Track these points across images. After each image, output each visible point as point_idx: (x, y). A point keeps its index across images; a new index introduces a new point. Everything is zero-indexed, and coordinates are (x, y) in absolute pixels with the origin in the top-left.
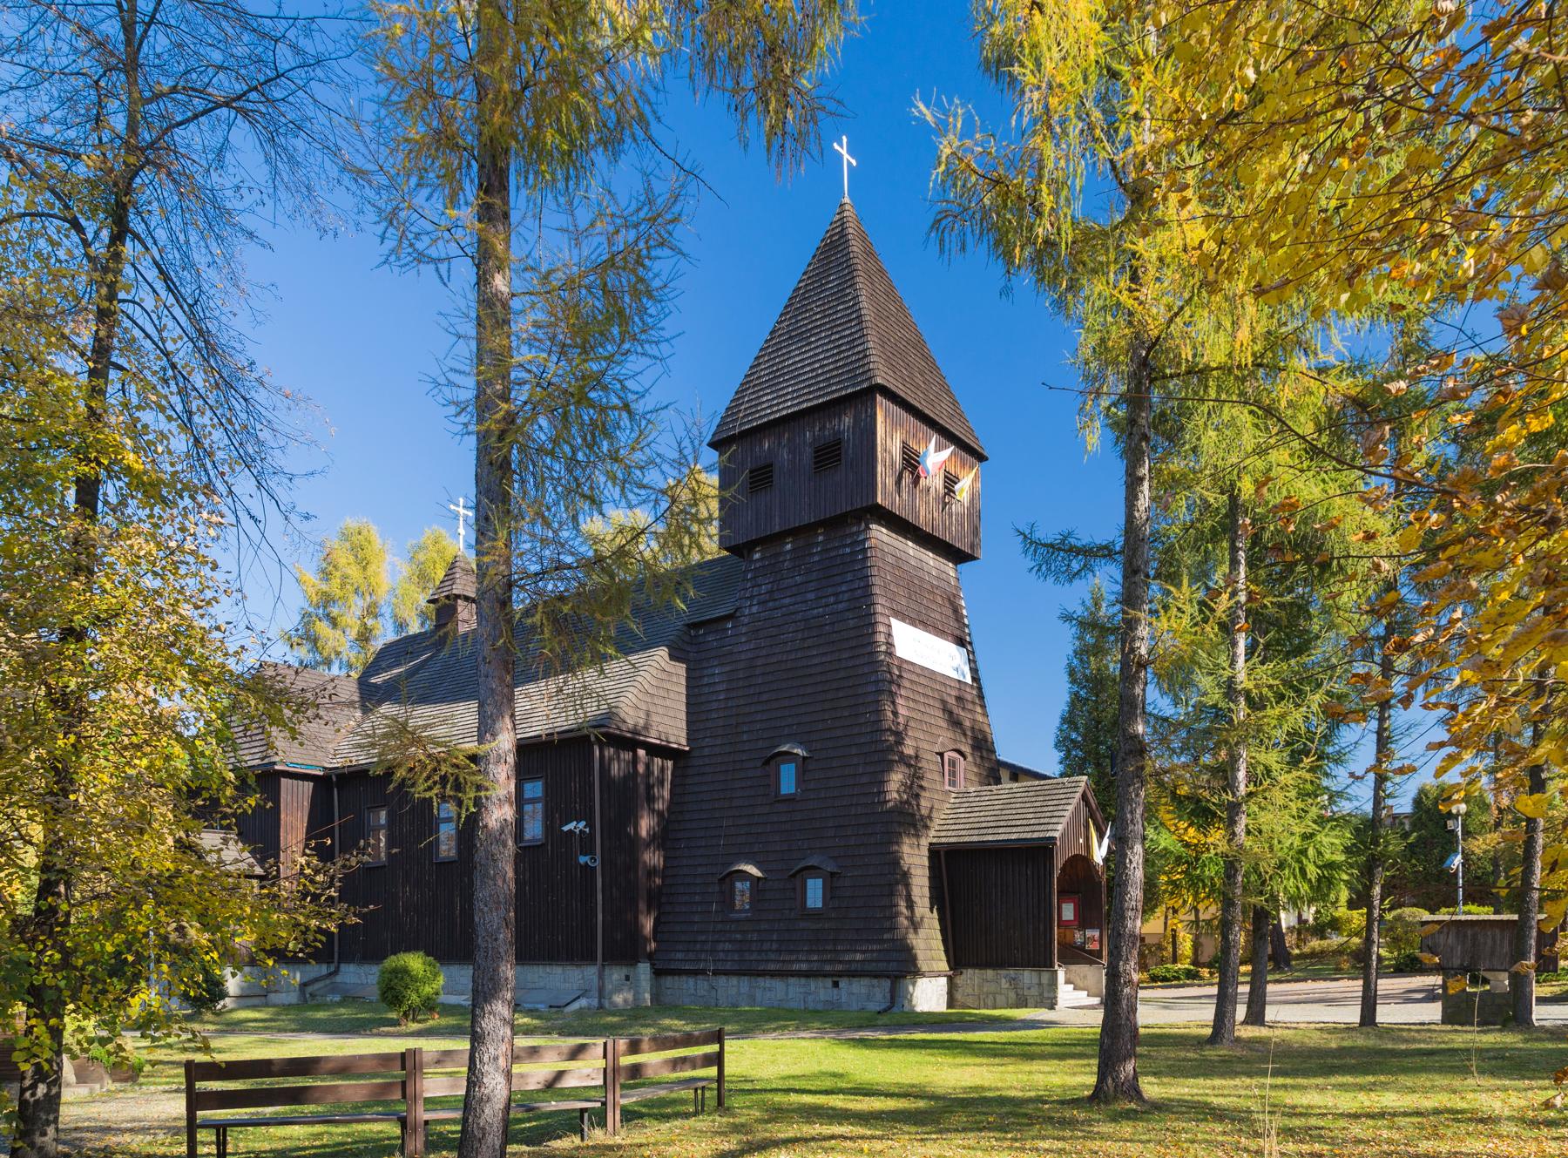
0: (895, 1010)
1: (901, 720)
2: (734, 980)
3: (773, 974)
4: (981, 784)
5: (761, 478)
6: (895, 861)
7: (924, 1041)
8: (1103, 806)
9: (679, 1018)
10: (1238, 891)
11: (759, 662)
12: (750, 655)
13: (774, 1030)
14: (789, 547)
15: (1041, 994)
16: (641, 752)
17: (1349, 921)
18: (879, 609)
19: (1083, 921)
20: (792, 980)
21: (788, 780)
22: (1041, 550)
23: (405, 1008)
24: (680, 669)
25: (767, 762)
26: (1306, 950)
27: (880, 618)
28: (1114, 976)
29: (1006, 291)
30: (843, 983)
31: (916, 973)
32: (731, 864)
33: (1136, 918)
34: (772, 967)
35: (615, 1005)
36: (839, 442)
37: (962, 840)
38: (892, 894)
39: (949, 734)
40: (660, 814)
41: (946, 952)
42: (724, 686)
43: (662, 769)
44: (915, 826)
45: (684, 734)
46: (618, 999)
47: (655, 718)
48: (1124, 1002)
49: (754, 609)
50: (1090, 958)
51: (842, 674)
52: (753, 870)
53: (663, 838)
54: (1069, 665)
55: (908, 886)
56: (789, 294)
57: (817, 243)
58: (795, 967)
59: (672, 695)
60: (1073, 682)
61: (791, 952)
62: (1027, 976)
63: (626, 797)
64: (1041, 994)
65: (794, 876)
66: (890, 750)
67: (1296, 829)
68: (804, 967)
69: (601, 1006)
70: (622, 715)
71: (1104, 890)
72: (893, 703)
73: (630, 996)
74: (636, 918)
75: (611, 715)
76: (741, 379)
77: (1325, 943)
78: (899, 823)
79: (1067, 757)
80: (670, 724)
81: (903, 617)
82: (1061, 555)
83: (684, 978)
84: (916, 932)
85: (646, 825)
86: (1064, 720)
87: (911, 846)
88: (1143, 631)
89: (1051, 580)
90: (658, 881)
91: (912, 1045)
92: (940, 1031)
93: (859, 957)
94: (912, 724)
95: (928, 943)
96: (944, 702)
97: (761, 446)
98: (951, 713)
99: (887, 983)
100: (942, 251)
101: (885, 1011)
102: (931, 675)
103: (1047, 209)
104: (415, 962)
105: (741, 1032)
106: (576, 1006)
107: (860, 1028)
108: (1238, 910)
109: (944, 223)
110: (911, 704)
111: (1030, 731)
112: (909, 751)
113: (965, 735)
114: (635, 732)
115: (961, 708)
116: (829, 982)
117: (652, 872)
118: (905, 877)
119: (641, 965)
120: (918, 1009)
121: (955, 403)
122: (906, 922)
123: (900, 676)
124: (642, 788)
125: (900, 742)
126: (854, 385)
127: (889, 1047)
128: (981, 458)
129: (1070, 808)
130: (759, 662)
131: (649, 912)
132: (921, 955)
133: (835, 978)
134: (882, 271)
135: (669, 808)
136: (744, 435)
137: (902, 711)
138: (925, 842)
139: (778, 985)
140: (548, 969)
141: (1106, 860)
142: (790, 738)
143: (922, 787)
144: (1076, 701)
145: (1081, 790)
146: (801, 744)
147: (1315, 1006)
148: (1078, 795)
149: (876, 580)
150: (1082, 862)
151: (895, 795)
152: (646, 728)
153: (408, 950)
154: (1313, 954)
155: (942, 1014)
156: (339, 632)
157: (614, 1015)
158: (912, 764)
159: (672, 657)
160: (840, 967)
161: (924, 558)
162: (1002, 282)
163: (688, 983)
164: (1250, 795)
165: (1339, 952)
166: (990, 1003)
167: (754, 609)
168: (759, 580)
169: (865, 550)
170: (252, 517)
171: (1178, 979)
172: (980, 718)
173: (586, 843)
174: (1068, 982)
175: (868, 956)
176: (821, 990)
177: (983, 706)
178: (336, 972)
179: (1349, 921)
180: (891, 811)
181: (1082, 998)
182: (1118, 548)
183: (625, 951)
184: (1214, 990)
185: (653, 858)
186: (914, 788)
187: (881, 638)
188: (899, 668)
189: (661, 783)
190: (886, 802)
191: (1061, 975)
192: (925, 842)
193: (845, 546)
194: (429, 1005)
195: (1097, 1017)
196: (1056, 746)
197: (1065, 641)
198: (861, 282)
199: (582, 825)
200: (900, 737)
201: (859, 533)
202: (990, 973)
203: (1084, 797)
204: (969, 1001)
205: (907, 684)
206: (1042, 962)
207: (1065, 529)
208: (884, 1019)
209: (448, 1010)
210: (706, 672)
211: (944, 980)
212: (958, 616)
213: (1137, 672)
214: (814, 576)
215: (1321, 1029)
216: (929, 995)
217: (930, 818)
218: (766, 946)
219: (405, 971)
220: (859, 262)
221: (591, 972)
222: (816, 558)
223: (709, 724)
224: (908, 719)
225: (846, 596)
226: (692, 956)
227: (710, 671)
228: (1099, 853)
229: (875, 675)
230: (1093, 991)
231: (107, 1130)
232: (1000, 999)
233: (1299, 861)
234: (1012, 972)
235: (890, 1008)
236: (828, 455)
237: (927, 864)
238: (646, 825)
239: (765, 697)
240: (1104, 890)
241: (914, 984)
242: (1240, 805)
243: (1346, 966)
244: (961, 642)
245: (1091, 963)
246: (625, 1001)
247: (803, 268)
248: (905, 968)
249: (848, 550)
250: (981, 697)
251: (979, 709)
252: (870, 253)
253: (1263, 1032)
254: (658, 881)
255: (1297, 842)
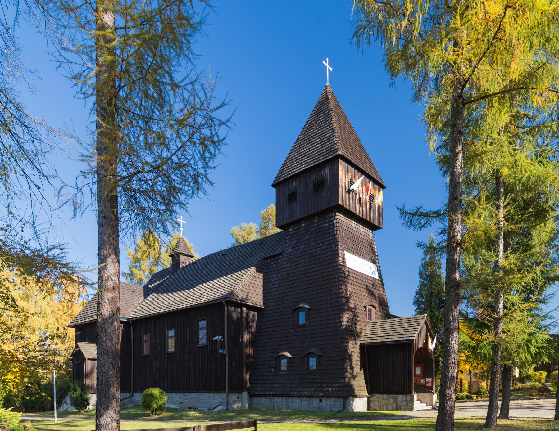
0: (345, 411)
1: (348, 292)
2: (280, 399)
3: (295, 396)
4: (382, 319)
5: (292, 197)
6: (346, 350)
7: (355, 424)
8: (433, 328)
9: (257, 414)
10: (499, 359)
11: (291, 272)
12: (287, 269)
13: (294, 419)
14: (303, 225)
15: (407, 405)
16: (244, 309)
17: (535, 376)
18: (340, 247)
19: (425, 375)
20: (303, 399)
21: (302, 318)
22: (408, 216)
23: (152, 409)
24: (261, 276)
25: (294, 311)
26: (516, 387)
27: (340, 251)
28: (443, 397)
29: (392, 85)
30: (324, 400)
31: (355, 396)
32: (280, 352)
33: (454, 368)
34: (295, 393)
35: (234, 408)
36: (323, 180)
37: (373, 341)
38: (344, 363)
39: (369, 299)
40: (252, 333)
41: (367, 387)
42: (278, 282)
43: (254, 316)
44: (354, 336)
45: (262, 301)
46: (235, 406)
47: (250, 295)
48: (448, 409)
49: (290, 251)
50: (428, 390)
51: (324, 275)
52: (288, 355)
53: (253, 343)
54: (420, 270)
55: (351, 361)
56: (305, 124)
57: (317, 103)
58: (305, 393)
59: (257, 286)
60: (421, 277)
61: (303, 387)
62: (401, 397)
63: (238, 326)
64: (407, 405)
65: (304, 357)
66: (344, 304)
67: (527, 331)
68: (308, 393)
69: (227, 409)
70: (236, 294)
71: (434, 361)
72: (346, 286)
73: (240, 405)
74: (242, 374)
75: (232, 293)
76: (285, 159)
77: (524, 385)
78: (347, 334)
79: (418, 308)
80: (256, 298)
81: (350, 251)
82: (417, 217)
83: (261, 398)
84: (354, 379)
85: (246, 337)
86: (417, 293)
87: (353, 344)
88: (459, 227)
89: (412, 228)
90: (251, 360)
91: (350, 426)
92: (362, 420)
93: (330, 389)
94: (353, 294)
95: (359, 384)
96: (367, 286)
97: (292, 184)
98: (370, 291)
99: (341, 400)
100: (358, 47)
101: (341, 411)
102: (362, 275)
103: (408, 12)
104: (156, 391)
105: (281, 420)
106: (218, 409)
107: (329, 418)
108: (499, 367)
109: (359, 32)
110: (353, 286)
111: (403, 303)
112: (352, 305)
113: (376, 299)
114: (242, 300)
115: (375, 290)
116: (318, 400)
117: (248, 356)
118: (350, 357)
119: (244, 393)
120: (355, 411)
121: (372, 165)
122: (350, 375)
123: (348, 275)
124: (245, 324)
125: (348, 302)
126: (329, 156)
127: (340, 427)
128: (383, 187)
129: (420, 327)
130: (291, 272)
131: (247, 372)
132: (356, 389)
133: (321, 398)
134: (342, 112)
135: (256, 331)
136: (286, 180)
137: (349, 289)
138: (358, 342)
139: (298, 400)
140: (208, 394)
141: (435, 349)
142: (303, 301)
143: (357, 320)
144: (422, 285)
145: (424, 320)
146: (307, 303)
147: (524, 410)
148: (423, 322)
149: (339, 236)
150: (424, 350)
151: (346, 323)
152: (247, 299)
153: (153, 387)
154: (519, 389)
155: (365, 413)
156: (142, 272)
157: (231, 412)
158: (353, 311)
159: (257, 271)
160: (322, 393)
161: (359, 228)
162: (390, 81)
163: (263, 400)
164: (505, 315)
165: (531, 388)
166: (385, 408)
167: (290, 251)
168: (292, 239)
169: (334, 224)
170: (36, 186)
171: (463, 399)
172: (382, 293)
173: (222, 344)
174: (418, 400)
175: (334, 389)
176: (315, 403)
177: (383, 288)
178: (132, 396)
179: (535, 376)
180: (344, 329)
181: (424, 406)
182: (442, 212)
183: (237, 387)
184: (487, 403)
185: (250, 351)
186: (354, 321)
187: (340, 259)
188: (348, 272)
189: (253, 321)
190: (342, 326)
191: (415, 397)
192: (358, 342)
193: (326, 223)
194: (161, 408)
195: (435, 414)
196: (414, 304)
197: (418, 257)
198: (333, 115)
199: (220, 337)
200: (348, 299)
201: (332, 217)
202: (385, 396)
203: (426, 323)
204: (376, 408)
205: (351, 278)
206: (407, 391)
207: (418, 205)
208: (340, 415)
209: (169, 410)
210: (270, 277)
211: (366, 399)
212: (374, 253)
213: (456, 247)
214: (313, 236)
215: (536, 421)
216: (359, 405)
217: (360, 333)
218: (293, 385)
219: (152, 395)
220: (333, 108)
221: (224, 395)
222: (314, 229)
223: (272, 297)
224: (351, 292)
225: (326, 243)
226: (264, 389)
227: (271, 276)
228: (432, 346)
229: (338, 275)
230: (429, 403)
231: (309, 423)
232: (389, 407)
233: (527, 345)
234: (394, 396)
235: (343, 410)
236: (319, 186)
237: (359, 351)
238: (246, 337)
239: (294, 285)
240: (434, 361)
241: (353, 401)
242: (500, 319)
243: (535, 394)
244: (374, 262)
245: (428, 392)
246: (238, 407)
247: (311, 113)
248: (350, 393)
249: (327, 224)
250: (383, 285)
251: (381, 289)
252: (337, 105)
253: (508, 422)
254: (251, 360)
255: (526, 337)
